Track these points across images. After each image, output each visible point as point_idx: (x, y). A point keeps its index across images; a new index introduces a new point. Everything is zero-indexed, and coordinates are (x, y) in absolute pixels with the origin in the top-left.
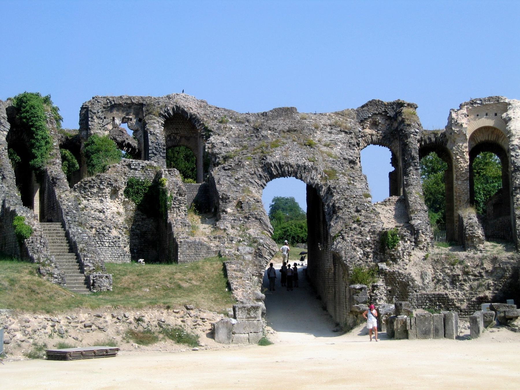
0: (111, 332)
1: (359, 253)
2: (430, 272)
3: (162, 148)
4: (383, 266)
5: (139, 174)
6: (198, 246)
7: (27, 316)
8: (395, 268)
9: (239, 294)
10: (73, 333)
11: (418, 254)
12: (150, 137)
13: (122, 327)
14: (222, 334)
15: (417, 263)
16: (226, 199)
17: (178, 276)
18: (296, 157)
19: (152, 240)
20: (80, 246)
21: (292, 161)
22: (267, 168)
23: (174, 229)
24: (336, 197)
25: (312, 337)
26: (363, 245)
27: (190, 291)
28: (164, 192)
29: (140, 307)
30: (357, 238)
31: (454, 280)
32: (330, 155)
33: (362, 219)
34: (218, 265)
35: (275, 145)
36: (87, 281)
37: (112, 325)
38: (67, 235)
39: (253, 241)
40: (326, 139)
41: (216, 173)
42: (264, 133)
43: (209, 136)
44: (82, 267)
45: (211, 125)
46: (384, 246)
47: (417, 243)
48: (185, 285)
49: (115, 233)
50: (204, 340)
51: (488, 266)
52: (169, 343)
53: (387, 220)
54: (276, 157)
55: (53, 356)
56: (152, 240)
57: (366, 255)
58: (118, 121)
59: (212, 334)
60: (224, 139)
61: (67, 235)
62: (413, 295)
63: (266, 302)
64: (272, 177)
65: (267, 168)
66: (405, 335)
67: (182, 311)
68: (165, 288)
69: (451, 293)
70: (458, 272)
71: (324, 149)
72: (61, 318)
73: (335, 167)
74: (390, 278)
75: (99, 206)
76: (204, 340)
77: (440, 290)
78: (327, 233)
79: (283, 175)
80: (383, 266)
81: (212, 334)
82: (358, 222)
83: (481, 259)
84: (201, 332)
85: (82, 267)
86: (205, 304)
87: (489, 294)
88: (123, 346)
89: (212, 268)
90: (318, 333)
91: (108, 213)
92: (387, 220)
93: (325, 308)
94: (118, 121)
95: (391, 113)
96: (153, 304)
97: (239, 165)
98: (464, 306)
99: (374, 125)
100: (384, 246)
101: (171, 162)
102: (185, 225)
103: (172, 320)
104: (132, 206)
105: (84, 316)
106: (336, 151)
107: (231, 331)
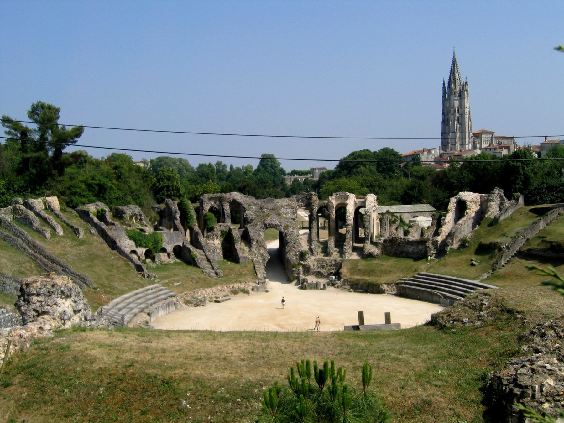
0: (226, 291)
1: (295, 258)
2: (316, 264)
3: (230, 215)
4: (302, 262)
5: (224, 229)
6: (246, 258)
7: (206, 289)
8: (306, 263)
9: (259, 276)
10: (217, 293)
11: (313, 258)
12: (225, 211)
13: (229, 290)
14: (255, 289)
15: (311, 261)
16: (253, 239)
17: (241, 270)
18: (274, 220)
19: (230, 253)
20: (211, 261)
21: (274, 223)
22: (265, 225)
23: (238, 251)
24: (288, 237)
25: (280, 284)
26: (296, 255)
27: (245, 275)
28: (233, 237)
29: (233, 283)
30: (294, 253)
31: (323, 267)
32: (286, 218)
33: (296, 246)
34: (252, 265)
35: (268, 216)
36: (216, 273)
37: (226, 289)
38: (206, 255)
39: (262, 255)
40: (285, 212)
41: (249, 227)
42: (264, 210)
43: (245, 211)
44: (213, 268)
45: (246, 206)
46: (302, 256)
47: (312, 254)
48: (243, 273)
49: (218, 251)
50: (251, 292)
51: (333, 262)
52: (241, 294)
53: (305, 247)
54: (268, 221)
55: (216, 302)
56: (230, 253)
57: (297, 259)
58: (213, 203)
59: (253, 290)
60: (250, 212)
61: (206, 255)
62: (311, 271)
63: (266, 274)
64: (267, 228)
65: (265, 225)
66: (305, 288)
67: (244, 283)
68: (238, 274)
69: (322, 271)
70: (324, 264)
71: (284, 216)
72: (214, 289)
73: (288, 223)
74: (304, 266)
75: (213, 242)
76: (251, 292)
77: (319, 270)
78: (285, 251)
79: (271, 227)
80: (302, 262)
81: (253, 290)
82: (294, 247)
83: (332, 260)
84: (250, 289)
85: (213, 268)
86: (250, 279)
87: (333, 271)
88: (231, 296)
89: (250, 266)
90: (283, 282)
91: (216, 244)
92: (305, 247)
93: (285, 269)
94: (213, 203)
95: (308, 197)
96: (236, 282)
97: (256, 224)
98: (326, 275)
99: (302, 201)
100: (302, 256)
101: (234, 222)
102: (240, 247)
103: (242, 286)
104: (222, 239)
105: (219, 287)
106: (289, 216)
107: (258, 288)
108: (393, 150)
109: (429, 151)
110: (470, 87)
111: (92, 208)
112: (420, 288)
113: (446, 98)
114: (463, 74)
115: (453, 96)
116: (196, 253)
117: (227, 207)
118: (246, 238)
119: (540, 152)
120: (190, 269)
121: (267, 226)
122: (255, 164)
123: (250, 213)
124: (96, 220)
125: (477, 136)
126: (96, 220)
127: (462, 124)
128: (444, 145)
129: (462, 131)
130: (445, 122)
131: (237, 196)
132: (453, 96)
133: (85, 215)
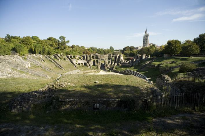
19: (94, 65)
54: (102, 59)
108: (174, 40)
109: (140, 47)
110: (149, 35)
111: (69, 56)
112: (175, 100)
113: (144, 37)
114: (148, 32)
115: (146, 37)
116: (88, 64)
117: (95, 56)
118: (97, 62)
119: (191, 93)
120: (86, 67)
121: (102, 60)
122: (109, 48)
123: (99, 57)
124: (70, 58)
125: (150, 44)
126: (70, 58)
127: (147, 42)
128: (143, 46)
129: (147, 43)
130: (144, 42)
131: (97, 54)
132: (146, 37)
133: (68, 57)
